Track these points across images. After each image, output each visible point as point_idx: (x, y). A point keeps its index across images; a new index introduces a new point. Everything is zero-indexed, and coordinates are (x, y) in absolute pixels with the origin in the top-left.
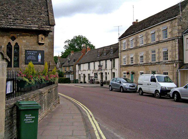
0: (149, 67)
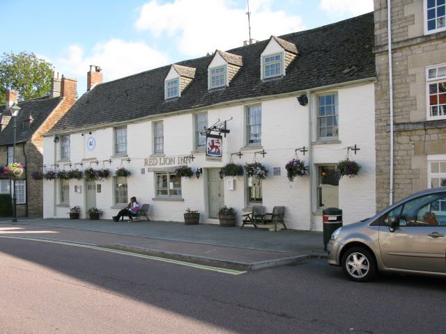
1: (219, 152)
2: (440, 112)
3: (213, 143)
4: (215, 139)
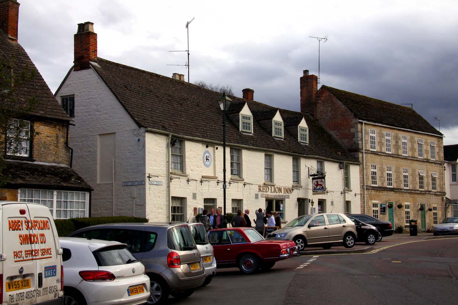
0: (417, 196)
1: (323, 188)
2: (73, 207)
3: (207, 158)
4: (318, 180)
